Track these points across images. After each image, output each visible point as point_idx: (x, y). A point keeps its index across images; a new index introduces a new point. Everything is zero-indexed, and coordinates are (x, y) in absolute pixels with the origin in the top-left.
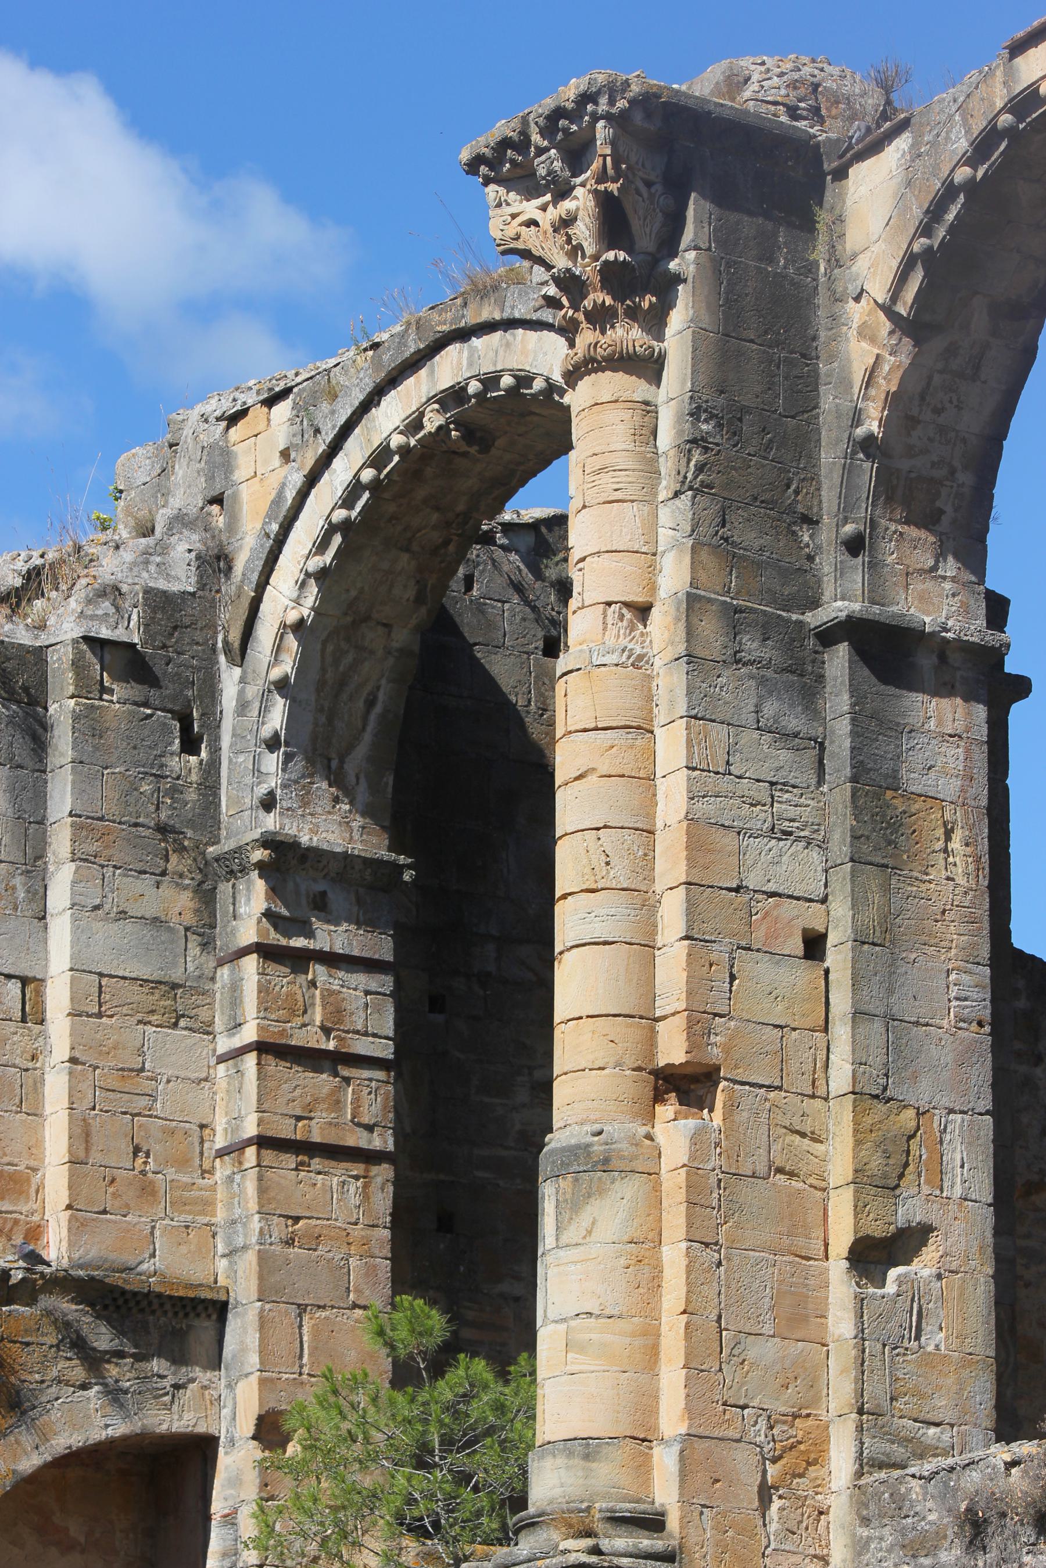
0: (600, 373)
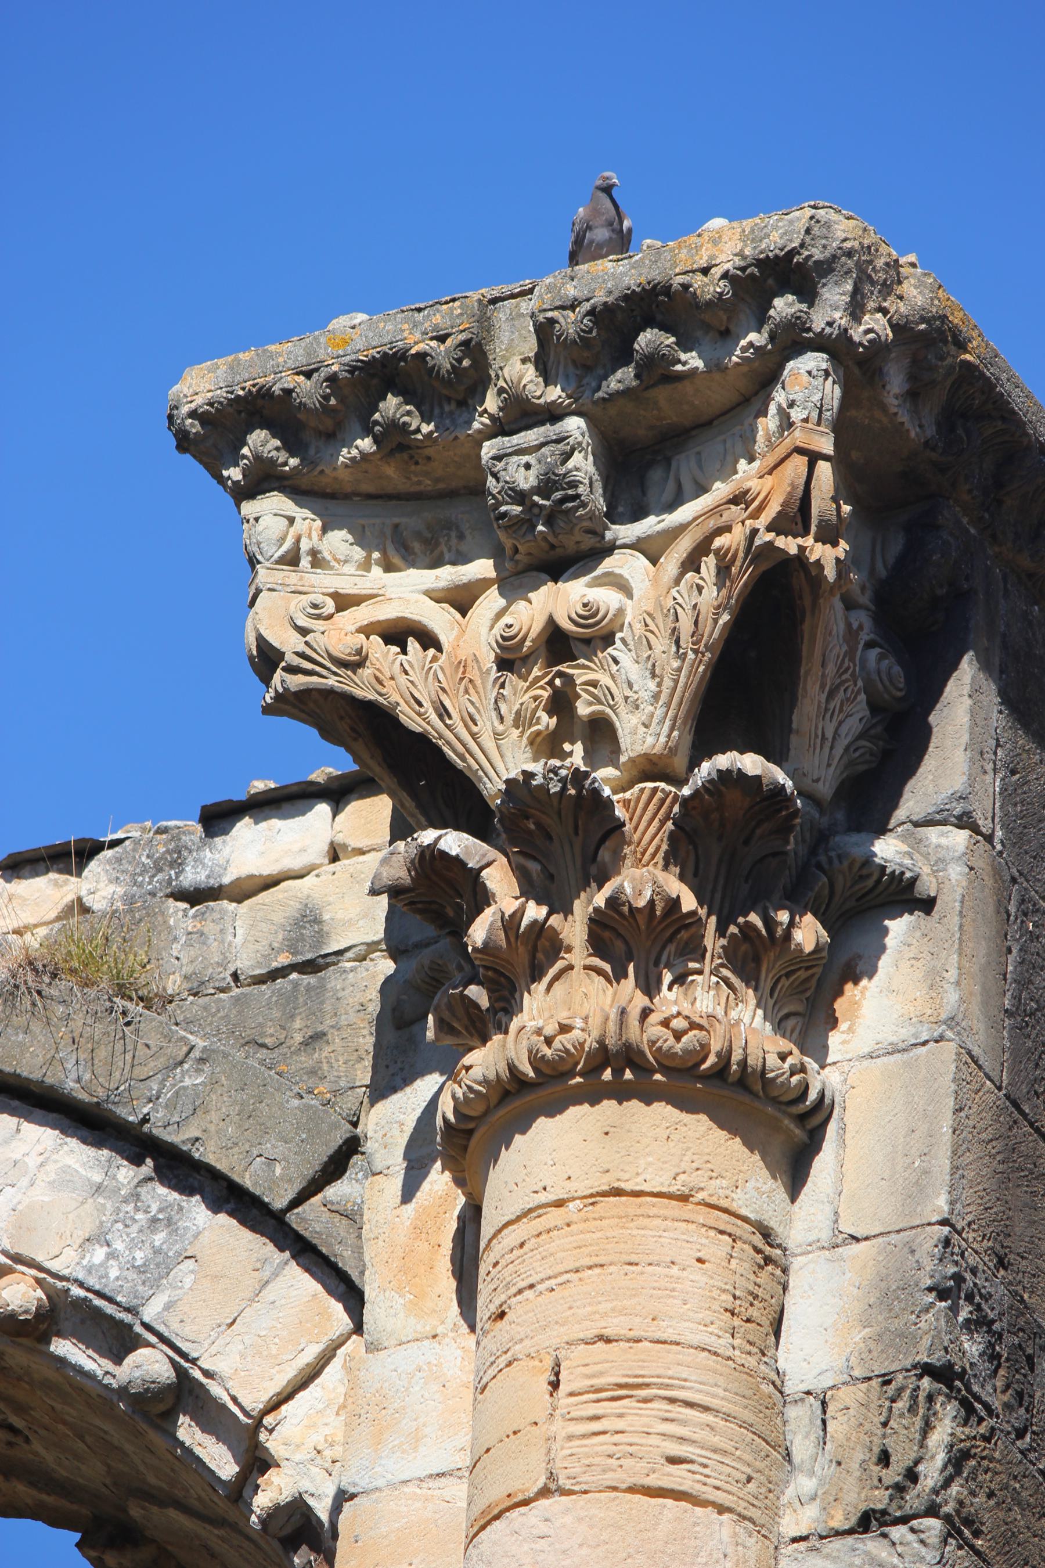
0: (635, 1104)
